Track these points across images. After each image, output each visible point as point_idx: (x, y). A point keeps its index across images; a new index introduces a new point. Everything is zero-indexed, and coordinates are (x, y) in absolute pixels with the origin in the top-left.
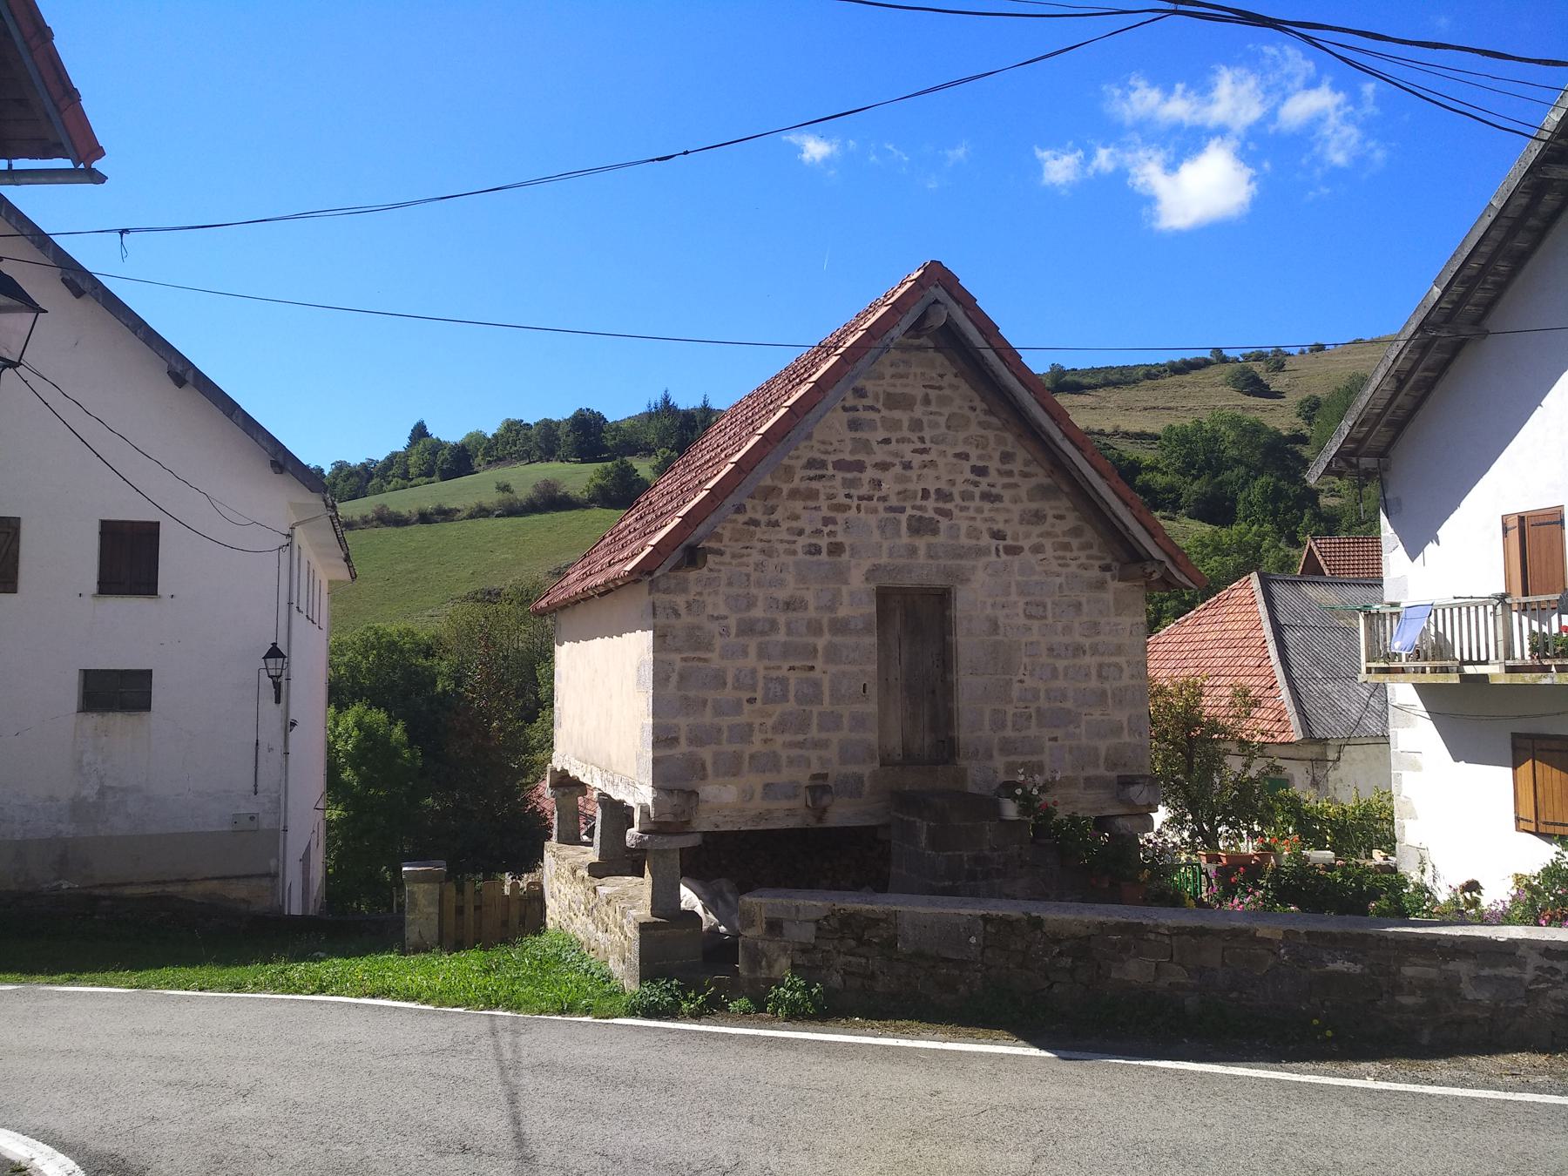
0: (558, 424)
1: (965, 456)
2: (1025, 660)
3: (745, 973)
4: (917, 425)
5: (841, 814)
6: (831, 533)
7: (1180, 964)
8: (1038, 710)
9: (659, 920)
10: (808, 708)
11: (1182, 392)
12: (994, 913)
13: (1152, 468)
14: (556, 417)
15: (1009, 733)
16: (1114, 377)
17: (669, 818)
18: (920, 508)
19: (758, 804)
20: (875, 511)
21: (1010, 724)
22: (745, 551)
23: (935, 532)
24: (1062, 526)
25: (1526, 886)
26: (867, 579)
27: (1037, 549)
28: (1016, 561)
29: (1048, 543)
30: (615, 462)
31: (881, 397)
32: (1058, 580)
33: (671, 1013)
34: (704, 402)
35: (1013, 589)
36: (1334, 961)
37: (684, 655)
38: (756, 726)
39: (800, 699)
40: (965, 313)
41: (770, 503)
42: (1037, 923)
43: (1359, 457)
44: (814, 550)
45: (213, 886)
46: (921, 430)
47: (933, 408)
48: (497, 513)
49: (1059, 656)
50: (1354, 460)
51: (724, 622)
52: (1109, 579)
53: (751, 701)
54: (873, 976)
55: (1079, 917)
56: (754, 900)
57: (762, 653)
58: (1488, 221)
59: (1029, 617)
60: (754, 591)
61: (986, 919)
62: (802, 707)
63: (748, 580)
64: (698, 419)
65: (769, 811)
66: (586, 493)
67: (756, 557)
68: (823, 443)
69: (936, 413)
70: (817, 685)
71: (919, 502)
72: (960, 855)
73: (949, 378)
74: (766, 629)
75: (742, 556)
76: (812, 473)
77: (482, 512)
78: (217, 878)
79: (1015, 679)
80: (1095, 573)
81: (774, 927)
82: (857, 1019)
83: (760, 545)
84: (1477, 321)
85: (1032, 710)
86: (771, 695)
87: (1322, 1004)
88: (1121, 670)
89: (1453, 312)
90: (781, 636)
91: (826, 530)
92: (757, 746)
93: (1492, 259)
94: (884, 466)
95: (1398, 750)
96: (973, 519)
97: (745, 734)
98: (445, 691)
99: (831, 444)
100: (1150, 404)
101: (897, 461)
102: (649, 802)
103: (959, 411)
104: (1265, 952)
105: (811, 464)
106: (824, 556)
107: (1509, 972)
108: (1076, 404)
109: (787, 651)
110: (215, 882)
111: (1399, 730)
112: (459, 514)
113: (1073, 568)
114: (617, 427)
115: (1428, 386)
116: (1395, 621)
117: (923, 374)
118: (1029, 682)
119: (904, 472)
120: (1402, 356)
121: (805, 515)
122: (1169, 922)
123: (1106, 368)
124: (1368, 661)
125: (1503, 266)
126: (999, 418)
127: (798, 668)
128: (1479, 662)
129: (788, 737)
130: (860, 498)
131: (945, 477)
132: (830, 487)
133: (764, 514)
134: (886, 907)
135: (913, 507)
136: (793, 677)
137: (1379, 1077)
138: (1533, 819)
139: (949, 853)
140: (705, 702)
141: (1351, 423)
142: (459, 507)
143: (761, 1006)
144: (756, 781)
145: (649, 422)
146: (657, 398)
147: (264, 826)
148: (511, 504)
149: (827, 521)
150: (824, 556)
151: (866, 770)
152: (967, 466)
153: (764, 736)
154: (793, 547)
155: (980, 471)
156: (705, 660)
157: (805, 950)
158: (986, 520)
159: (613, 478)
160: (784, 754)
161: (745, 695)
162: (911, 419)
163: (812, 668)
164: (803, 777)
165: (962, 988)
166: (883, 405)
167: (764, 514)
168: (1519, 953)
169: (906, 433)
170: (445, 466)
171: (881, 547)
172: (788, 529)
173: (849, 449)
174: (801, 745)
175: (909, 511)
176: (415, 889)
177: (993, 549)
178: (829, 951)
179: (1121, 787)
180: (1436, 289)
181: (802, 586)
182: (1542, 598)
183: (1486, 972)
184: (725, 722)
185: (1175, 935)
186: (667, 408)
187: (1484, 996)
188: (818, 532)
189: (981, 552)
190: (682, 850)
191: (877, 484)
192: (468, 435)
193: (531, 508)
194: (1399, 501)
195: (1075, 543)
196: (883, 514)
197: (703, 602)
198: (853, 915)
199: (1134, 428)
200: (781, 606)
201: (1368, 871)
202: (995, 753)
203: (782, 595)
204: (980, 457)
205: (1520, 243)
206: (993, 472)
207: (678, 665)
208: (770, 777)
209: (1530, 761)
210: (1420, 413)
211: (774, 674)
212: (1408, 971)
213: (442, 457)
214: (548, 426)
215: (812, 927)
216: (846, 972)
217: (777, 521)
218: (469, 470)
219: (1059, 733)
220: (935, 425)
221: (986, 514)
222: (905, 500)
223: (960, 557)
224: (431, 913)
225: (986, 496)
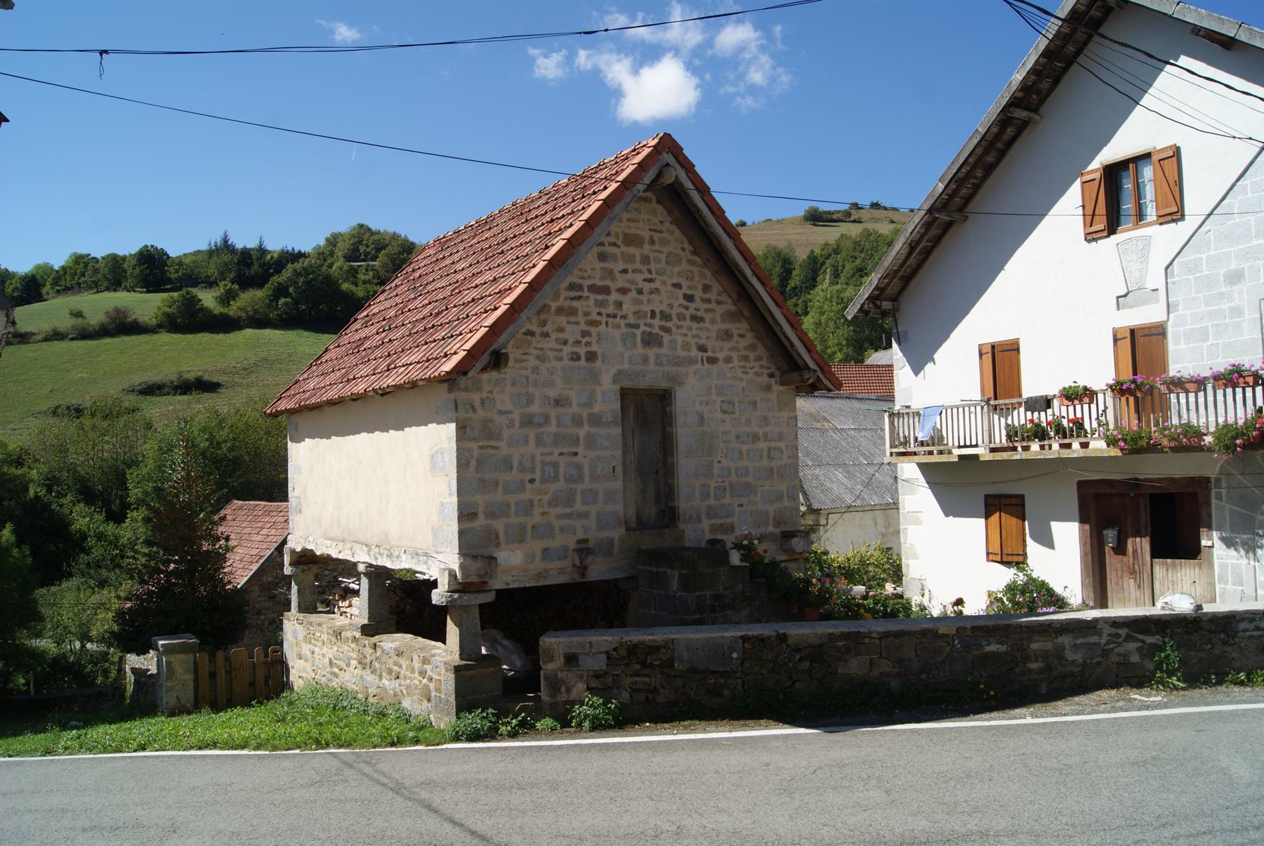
0: (124, 258)
1: (677, 286)
2: (722, 445)
3: (547, 699)
4: (646, 260)
5: (599, 570)
6: (588, 344)
7: (887, 659)
8: (731, 484)
9: (469, 663)
10: (573, 486)
12: (750, 633)
14: (121, 253)
15: (712, 502)
17: (475, 579)
18: (650, 326)
19: (538, 565)
20: (618, 326)
21: (712, 494)
22: (524, 357)
23: (660, 344)
24: (743, 343)
25: (995, 598)
26: (614, 381)
27: (728, 360)
28: (715, 369)
29: (735, 355)
30: (181, 293)
31: (621, 236)
32: (743, 384)
33: (492, 734)
34: (260, 242)
35: (713, 390)
36: (989, 645)
37: (481, 444)
38: (536, 502)
39: (569, 480)
40: (688, 176)
41: (543, 317)
42: (783, 638)
43: (881, 301)
44: (575, 357)
46: (649, 263)
47: (657, 247)
48: (70, 336)
49: (743, 442)
50: (878, 303)
51: (510, 416)
52: (773, 383)
53: (532, 481)
54: (655, 691)
55: (815, 632)
56: (553, 640)
57: (539, 442)
58: (975, 141)
59: (724, 412)
60: (532, 390)
61: (745, 639)
62: (570, 486)
63: (527, 381)
64: (254, 257)
65: (546, 571)
66: (154, 319)
67: (533, 362)
68: (580, 270)
69: (659, 251)
70: (579, 467)
71: (649, 321)
72: (705, 595)
73: (667, 225)
74: (542, 422)
75: (523, 361)
76: (573, 294)
77: (57, 336)
79: (716, 460)
80: (764, 379)
81: (571, 660)
82: (648, 724)
83: (535, 352)
84: (961, 209)
85: (726, 484)
86: (546, 476)
87: (981, 675)
88: (782, 452)
89: (948, 201)
90: (553, 428)
91: (584, 341)
92: (536, 518)
93: (974, 167)
94: (624, 291)
95: (906, 511)
96: (686, 335)
97: (528, 508)
98: (37, 498)
99: (586, 271)
101: (632, 287)
102: (456, 567)
103: (674, 251)
104: (944, 644)
105: (572, 287)
106: (583, 362)
107: (1093, 639)
109: (558, 440)
111: (906, 497)
112: (34, 338)
113: (751, 376)
114: (179, 262)
115: (928, 253)
116: (916, 419)
117: (649, 220)
118: (725, 463)
119: (638, 296)
120: (916, 230)
121: (569, 328)
122: (880, 629)
124: (891, 448)
125: (979, 173)
126: (702, 258)
127: (566, 454)
128: (971, 446)
129: (560, 510)
130: (608, 316)
131: (666, 302)
132: (586, 306)
133: (538, 326)
134: (666, 636)
135: (645, 325)
136: (562, 460)
137: (1032, 716)
138: (999, 553)
139: (698, 593)
140: (497, 483)
141: (879, 276)
142: (34, 331)
143: (565, 722)
144: (536, 546)
145: (210, 258)
146: (216, 238)
148: (84, 329)
149: (585, 334)
150: (583, 362)
151: (617, 534)
152: (680, 293)
153: (541, 511)
154: (560, 354)
155: (689, 298)
156: (496, 448)
157: (597, 676)
158: (694, 336)
159: (179, 307)
160: (557, 524)
161: (528, 477)
162: (642, 255)
163: (576, 454)
164: (570, 542)
165: (726, 692)
166: (622, 242)
167: (538, 326)
168: (1099, 626)
169: (638, 265)
170: (15, 294)
171: (623, 355)
172: (556, 339)
173: (599, 276)
174: (568, 516)
175: (643, 328)
176: (172, 659)
177: (700, 359)
178: (618, 675)
179: (784, 540)
180: (940, 184)
181: (567, 386)
182: (1007, 401)
183: (1080, 641)
184: (513, 499)
185: (883, 637)
186: (226, 246)
187: (1079, 657)
188: (578, 342)
189: (692, 361)
190: (481, 606)
191: (619, 305)
192: (35, 266)
193: (103, 332)
194: (906, 333)
195: (752, 356)
196: (624, 329)
197: (494, 399)
198: (636, 646)
200: (552, 402)
201: (887, 597)
202: (704, 517)
203: (553, 393)
204: (689, 287)
205: (990, 159)
206: (698, 300)
207: (476, 452)
208: (547, 543)
209: (998, 513)
210: (921, 271)
211: (549, 459)
212: (1034, 646)
213: (12, 287)
214: (115, 262)
215: (604, 656)
216: (633, 690)
217: (548, 332)
218: (38, 298)
219: (744, 500)
220: (658, 261)
221: (695, 332)
222: (639, 319)
223: (678, 365)
224: (187, 680)
225: (694, 318)
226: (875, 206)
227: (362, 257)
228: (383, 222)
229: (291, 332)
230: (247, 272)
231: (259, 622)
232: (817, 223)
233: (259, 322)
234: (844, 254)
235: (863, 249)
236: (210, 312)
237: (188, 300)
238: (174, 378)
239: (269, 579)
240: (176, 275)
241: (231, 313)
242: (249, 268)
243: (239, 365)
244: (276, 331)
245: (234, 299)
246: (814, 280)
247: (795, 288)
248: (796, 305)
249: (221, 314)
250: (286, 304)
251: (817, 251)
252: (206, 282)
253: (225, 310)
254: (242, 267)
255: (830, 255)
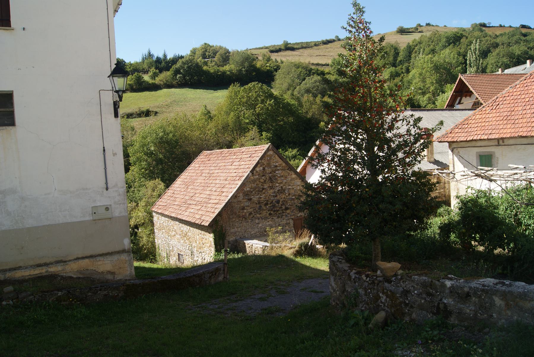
11: (327, 50)
13: (329, 73)
16: (304, 46)
45: (84, 263)
78: (87, 257)
100: (318, 54)
108: (293, 54)
110: (87, 260)
123: (301, 43)
147: (117, 214)
159: (134, 81)
199: (316, 62)
226: (428, 25)
227: (207, 57)
228: (215, 42)
229: (183, 89)
230: (160, 66)
231: (244, 214)
232: (403, 34)
233: (169, 86)
234: (424, 43)
235: (433, 41)
236: (148, 82)
237: (138, 77)
238: (137, 110)
239: (248, 189)
240: (130, 69)
241: (156, 83)
242: (161, 64)
243: (164, 104)
244: (177, 89)
245: (157, 76)
246: (410, 56)
247: (401, 61)
248: (402, 69)
249: (152, 83)
250: (179, 77)
251: (411, 44)
252: (142, 72)
253: (153, 81)
254: (157, 64)
255: (417, 45)
